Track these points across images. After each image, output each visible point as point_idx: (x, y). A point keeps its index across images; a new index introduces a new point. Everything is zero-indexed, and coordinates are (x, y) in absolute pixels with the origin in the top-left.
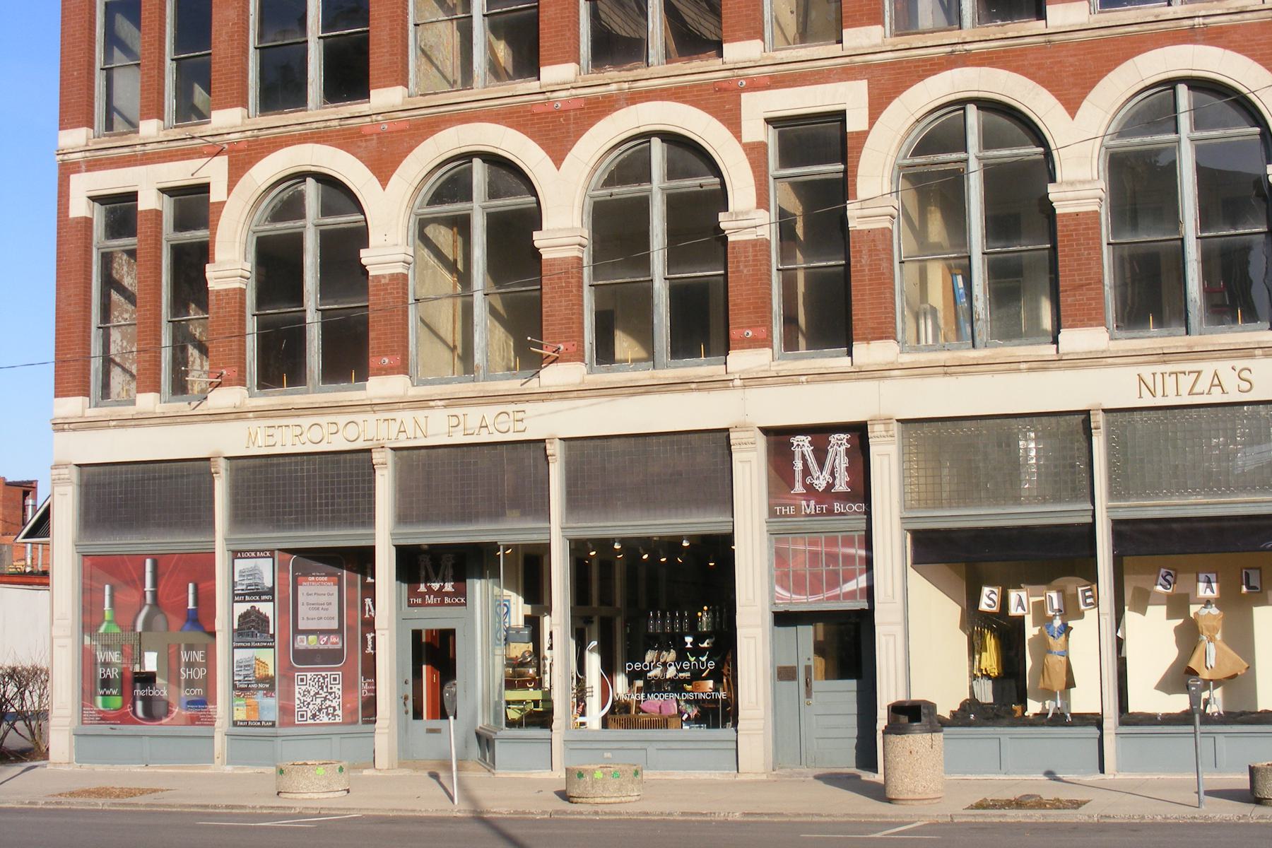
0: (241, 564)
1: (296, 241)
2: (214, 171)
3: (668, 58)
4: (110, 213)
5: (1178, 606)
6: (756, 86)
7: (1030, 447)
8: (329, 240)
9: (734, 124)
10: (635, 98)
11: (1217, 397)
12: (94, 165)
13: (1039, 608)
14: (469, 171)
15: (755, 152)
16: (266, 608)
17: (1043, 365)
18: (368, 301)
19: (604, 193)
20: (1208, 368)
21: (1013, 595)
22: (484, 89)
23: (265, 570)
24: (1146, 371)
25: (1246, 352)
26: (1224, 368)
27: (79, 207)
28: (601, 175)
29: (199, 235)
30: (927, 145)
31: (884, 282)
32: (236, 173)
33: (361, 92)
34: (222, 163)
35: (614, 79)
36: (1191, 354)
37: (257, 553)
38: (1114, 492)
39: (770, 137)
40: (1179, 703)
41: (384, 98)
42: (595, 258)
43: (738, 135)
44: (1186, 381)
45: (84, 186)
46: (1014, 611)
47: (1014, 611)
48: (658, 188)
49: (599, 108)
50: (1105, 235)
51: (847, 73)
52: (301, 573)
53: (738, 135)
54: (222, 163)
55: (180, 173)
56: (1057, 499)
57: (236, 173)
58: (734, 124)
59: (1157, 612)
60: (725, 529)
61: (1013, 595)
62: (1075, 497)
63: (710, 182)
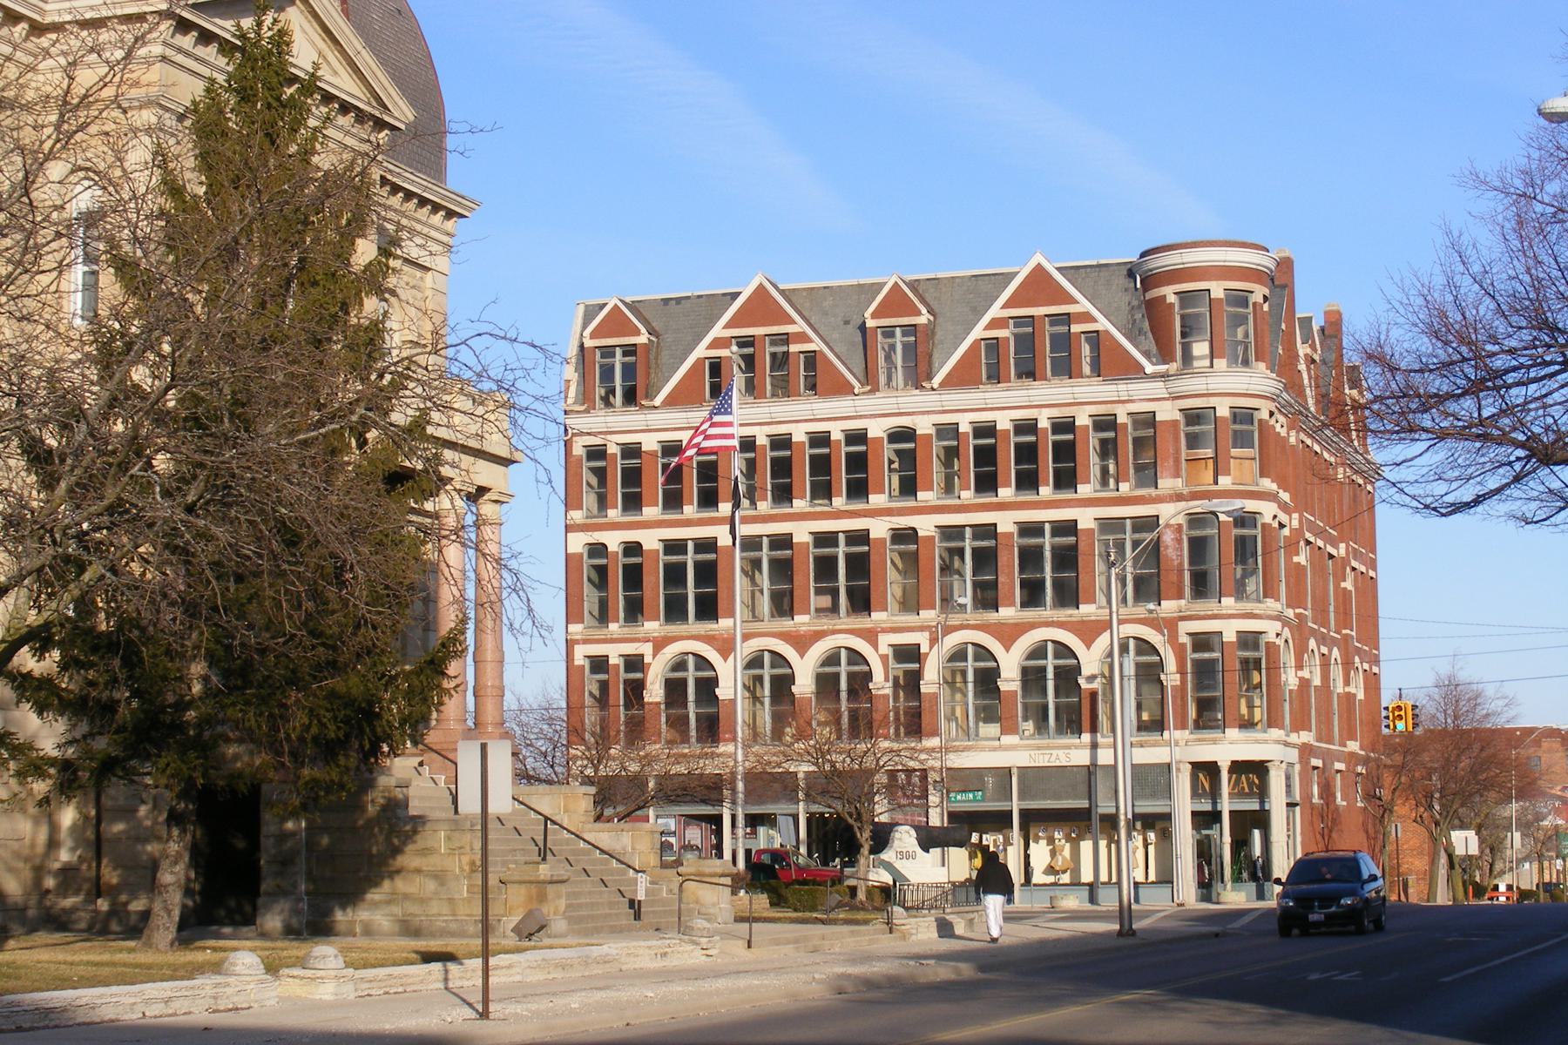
0: (660, 821)
1: (684, 682)
2: (646, 649)
3: (848, 614)
4: (591, 663)
5: (1051, 841)
6: (884, 631)
7: (990, 781)
8: (699, 682)
9: (876, 647)
10: (834, 632)
11: (1058, 764)
12: (586, 642)
13: (995, 841)
14: (763, 656)
15: (884, 658)
16: (672, 840)
17: (994, 749)
18: (1175, 728)
19: (821, 670)
20: (1054, 752)
21: (984, 836)
22: (973, 616)
23: (672, 824)
24: (1032, 753)
25: (1068, 747)
26: (1061, 753)
27: (579, 660)
28: (820, 662)
29: (639, 675)
30: (952, 658)
31: (935, 713)
32: (656, 651)
33: (791, 613)
34: (650, 645)
35: (1031, 614)
36: (1048, 748)
37: (668, 816)
38: (1021, 797)
39: (889, 652)
40: (1051, 879)
41: (1086, 610)
42: (817, 698)
43: (877, 650)
44: (1047, 757)
45: (581, 653)
46: (985, 842)
47: (985, 842)
48: (843, 669)
49: (818, 636)
50: (1019, 698)
51: (921, 629)
52: (687, 824)
53: (877, 650)
54: (650, 645)
55: (630, 649)
56: (999, 800)
57: (656, 651)
58: (875, 646)
59: (1043, 843)
60: (1166, 810)
61: (984, 836)
62: (1006, 800)
63: (866, 668)
